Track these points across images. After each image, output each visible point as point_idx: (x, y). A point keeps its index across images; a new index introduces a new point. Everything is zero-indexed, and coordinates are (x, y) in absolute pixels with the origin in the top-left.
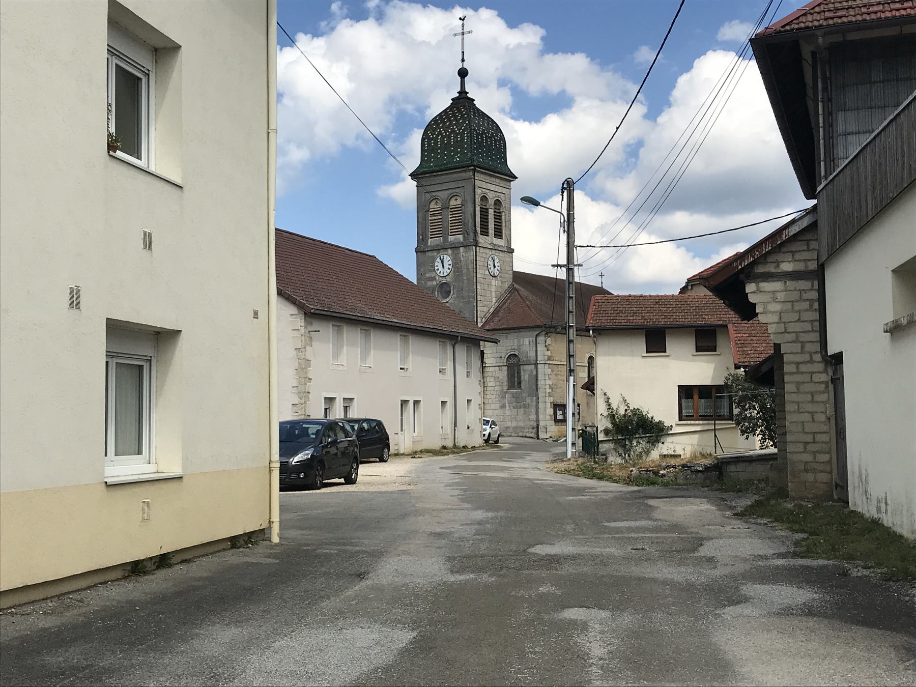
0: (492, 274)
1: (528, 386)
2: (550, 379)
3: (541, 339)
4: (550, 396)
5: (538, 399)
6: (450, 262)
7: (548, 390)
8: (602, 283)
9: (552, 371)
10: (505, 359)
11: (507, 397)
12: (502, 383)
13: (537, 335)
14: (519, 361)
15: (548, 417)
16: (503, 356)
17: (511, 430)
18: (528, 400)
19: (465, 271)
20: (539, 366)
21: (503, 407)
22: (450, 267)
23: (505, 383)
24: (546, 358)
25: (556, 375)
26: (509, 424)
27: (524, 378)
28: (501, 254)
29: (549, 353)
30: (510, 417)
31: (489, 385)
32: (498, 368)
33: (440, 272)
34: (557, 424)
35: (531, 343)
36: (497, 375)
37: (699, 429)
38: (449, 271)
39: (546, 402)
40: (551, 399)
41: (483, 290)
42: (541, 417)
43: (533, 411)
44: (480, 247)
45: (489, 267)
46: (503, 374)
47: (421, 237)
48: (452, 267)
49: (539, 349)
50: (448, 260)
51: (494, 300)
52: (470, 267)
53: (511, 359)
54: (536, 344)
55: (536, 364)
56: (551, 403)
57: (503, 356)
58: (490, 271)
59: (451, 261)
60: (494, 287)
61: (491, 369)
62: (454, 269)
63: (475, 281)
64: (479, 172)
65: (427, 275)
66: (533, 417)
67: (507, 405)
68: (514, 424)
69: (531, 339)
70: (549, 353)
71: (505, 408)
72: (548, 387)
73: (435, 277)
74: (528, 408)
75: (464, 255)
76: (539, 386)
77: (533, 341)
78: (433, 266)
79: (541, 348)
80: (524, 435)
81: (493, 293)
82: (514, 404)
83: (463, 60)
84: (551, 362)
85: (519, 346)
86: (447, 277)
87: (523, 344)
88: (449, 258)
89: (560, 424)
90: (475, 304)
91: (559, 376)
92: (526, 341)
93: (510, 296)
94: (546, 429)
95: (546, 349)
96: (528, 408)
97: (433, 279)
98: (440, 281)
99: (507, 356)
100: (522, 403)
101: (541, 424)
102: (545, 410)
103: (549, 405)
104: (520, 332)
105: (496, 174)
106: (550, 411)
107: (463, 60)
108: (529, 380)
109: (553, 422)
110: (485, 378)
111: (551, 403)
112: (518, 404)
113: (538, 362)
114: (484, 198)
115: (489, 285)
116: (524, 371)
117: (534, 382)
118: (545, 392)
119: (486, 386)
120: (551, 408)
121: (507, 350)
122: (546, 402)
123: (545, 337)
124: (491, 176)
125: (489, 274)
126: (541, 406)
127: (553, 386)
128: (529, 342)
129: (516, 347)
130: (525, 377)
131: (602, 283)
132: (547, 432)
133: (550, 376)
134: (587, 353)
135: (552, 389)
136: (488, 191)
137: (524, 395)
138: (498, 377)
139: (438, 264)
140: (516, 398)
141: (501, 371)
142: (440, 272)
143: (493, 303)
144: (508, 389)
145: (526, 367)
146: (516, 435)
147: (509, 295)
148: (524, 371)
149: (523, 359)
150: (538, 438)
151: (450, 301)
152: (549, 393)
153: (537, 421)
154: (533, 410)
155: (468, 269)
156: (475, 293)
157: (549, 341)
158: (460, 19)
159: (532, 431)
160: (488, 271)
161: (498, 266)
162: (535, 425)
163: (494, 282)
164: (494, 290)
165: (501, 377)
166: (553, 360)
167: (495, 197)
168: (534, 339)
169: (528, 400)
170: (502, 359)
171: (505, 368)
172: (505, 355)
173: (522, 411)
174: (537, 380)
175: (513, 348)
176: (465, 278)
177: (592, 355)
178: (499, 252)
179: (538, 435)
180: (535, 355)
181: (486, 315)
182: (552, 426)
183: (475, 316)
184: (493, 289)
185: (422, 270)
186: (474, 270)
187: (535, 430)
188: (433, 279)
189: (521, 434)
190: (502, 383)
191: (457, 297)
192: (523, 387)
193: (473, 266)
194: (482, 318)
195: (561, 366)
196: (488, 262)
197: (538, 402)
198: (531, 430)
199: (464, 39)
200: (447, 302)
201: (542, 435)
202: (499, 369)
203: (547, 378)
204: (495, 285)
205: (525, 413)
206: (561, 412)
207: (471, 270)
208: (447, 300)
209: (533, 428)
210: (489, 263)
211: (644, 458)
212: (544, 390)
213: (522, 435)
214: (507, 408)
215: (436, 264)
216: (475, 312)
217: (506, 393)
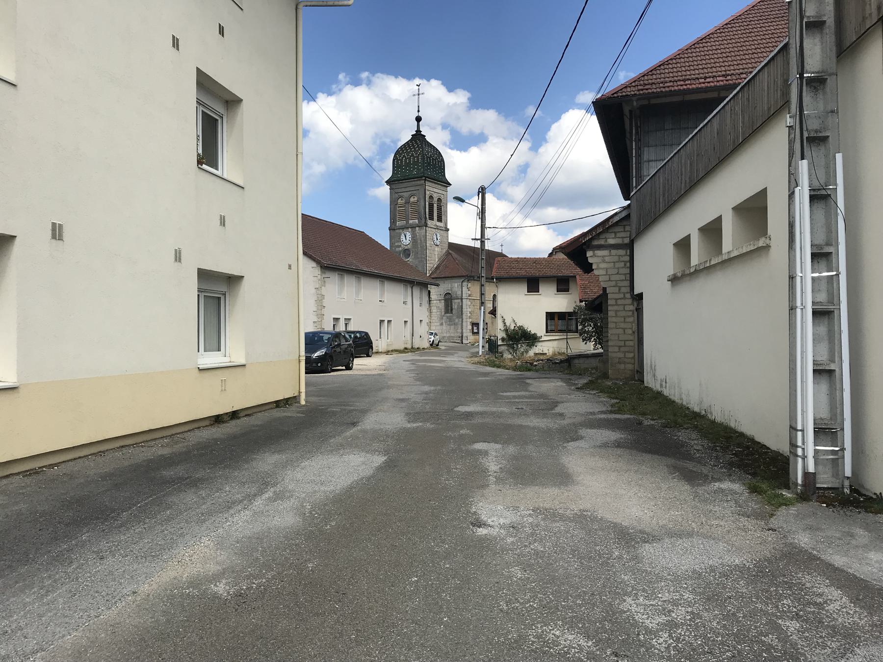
2: (469, 308)
6: (410, 236)
9: (472, 303)
15: (468, 331)
17: (446, 338)
18: (457, 321)
19: (419, 242)
21: (442, 324)
23: (443, 310)
25: (474, 306)
26: (445, 335)
28: (441, 232)
29: (469, 292)
40: (471, 320)
46: (442, 305)
50: (409, 235)
52: (423, 239)
61: (435, 302)
65: (396, 244)
66: (460, 331)
67: (444, 323)
70: (469, 292)
76: (463, 312)
78: (400, 238)
79: (465, 289)
81: (436, 256)
82: (448, 323)
84: (470, 298)
85: (452, 288)
94: (467, 337)
97: (400, 246)
101: (464, 335)
102: (467, 327)
103: (469, 323)
106: (470, 327)
107: (419, 111)
114: (431, 197)
115: (434, 250)
117: (460, 309)
126: (464, 324)
130: (455, 306)
139: (403, 237)
150: (462, 343)
153: (462, 333)
157: (470, 285)
162: (461, 335)
163: (437, 249)
168: (461, 284)
169: (457, 321)
173: (452, 327)
174: (462, 308)
184: (436, 253)
188: (400, 246)
189: (452, 341)
201: (464, 341)
203: (468, 307)
206: (476, 328)
209: (459, 337)
211: (525, 355)
215: (402, 237)
217: (444, 316)
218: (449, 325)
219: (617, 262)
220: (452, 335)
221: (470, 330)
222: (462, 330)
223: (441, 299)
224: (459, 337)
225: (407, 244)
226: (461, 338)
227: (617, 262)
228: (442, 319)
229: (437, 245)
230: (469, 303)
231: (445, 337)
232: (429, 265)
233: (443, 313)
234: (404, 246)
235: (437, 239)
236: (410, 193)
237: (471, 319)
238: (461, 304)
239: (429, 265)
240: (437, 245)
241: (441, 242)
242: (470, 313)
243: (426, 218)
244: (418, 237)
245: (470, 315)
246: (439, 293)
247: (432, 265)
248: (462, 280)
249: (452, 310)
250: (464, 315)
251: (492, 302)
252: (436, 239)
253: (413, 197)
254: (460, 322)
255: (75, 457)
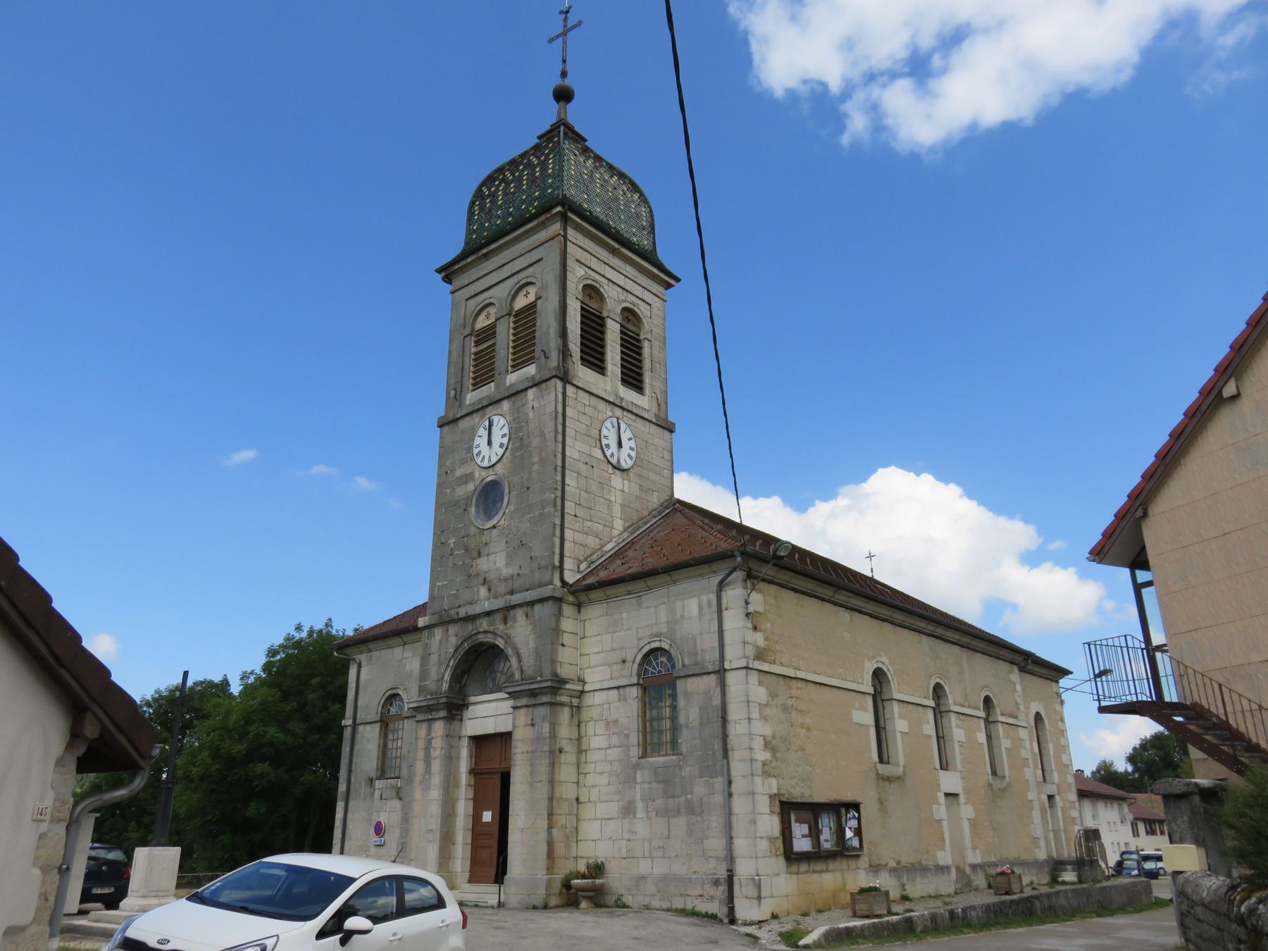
0: (614, 461)
1: (698, 741)
2: (764, 718)
3: (734, 594)
4: (767, 774)
5: (730, 782)
6: (506, 430)
7: (762, 755)
8: (872, 569)
9: (773, 695)
10: (636, 666)
11: (639, 778)
12: (627, 735)
13: (721, 585)
14: (673, 666)
15: (763, 845)
16: (629, 657)
17: (650, 888)
18: (699, 789)
19: (535, 441)
20: (731, 678)
21: (628, 810)
22: (505, 441)
23: (634, 739)
24: (750, 651)
25: (785, 709)
26: (644, 867)
27: (688, 717)
28: (640, 424)
29: (759, 639)
30: (646, 844)
31: (592, 746)
32: (615, 692)
33: (484, 457)
34: (794, 868)
35: (706, 610)
36: (614, 716)
37: (435, 794)
38: (500, 452)
39: (753, 794)
40: (773, 785)
41: (586, 491)
42: (740, 844)
43: (714, 825)
44: (578, 387)
45: (604, 442)
46: (627, 710)
47: (453, 393)
48: (510, 439)
49: (728, 625)
50: (501, 427)
51: (619, 525)
52: (549, 428)
53: (649, 663)
54: (720, 611)
55: (721, 672)
56: (772, 797)
57: (629, 657)
58: (608, 453)
59: (507, 426)
60: (618, 493)
61: (599, 698)
62: (513, 444)
63: (559, 463)
64: (578, 228)
65: (458, 473)
66: (716, 844)
67: (640, 804)
68: (659, 868)
69: (704, 599)
70: (759, 639)
71: (635, 814)
72: (758, 743)
73: (472, 474)
74: (700, 814)
75: (536, 405)
76: (733, 741)
77: (709, 606)
78: (470, 449)
79: (734, 621)
80: (689, 906)
81: (617, 510)
82: (660, 801)
83: (564, 74)
84: (765, 667)
85: (672, 623)
86: (499, 468)
87: (683, 617)
88: (503, 421)
89: (804, 867)
90: (558, 521)
91: (794, 714)
92: (692, 606)
93: (661, 523)
94: (758, 886)
95: (750, 625)
96: (700, 814)
97: (468, 478)
98: (483, 479)
99: (640, 656)
100: (683, 799)
101: (744, 869)
102: (754, 822)
103: (764, 804)
104: (674, 582)
105: (624, 250)
106: (770, 824)
107: (564, 74)
108: (701, 724)
109: (782, 860)
110: (583, 725)
111: (772, 797)
112: (671, 801)
113: (727, 666)
114: (591, 291)
115: (604, 484)
116: (688, 695)
117: (717, 727)
118: (752, 760)
119: (584, 748)
120: (772, 812)
121: (639, 639)
122: (753, 794)
123: (746, 588)
124: (613, 251)
125: (602, 457)
126: (739, 805)
127: (774, 742)
128: (701, 608)
129: (664, 629)
130: (690, 713)
131: (872, 569)
132: (759, 898)
133: (768, 711)
134: (870, 659)
135: (774, 751)
136: (606, 281)
137: (687, 771)
138: (616, 721)
139: (481, 441)
140: (667, 782)
141: (625, 700)
142: (484, 457)
143: (615, 533)
144: (644, 756)
145: (694, 685)
146: (665, 905)
147: (662, 520)
148: (688, 695)
149: (683, 660)
150: (733, 921)
151: (502, 522)
152: (764, 764)
153: (730, 858)
154: (716, 821)
155: (542, 434)
156: (559, 493)
157: (758, 601)
158: (561, 12)
159: (712, 893)
160: (600, 451)
161: (631, 449)
162: (722, 873)
163: (617, 481)
164: (619, 501)
165: (624, 721)
166: (774, 663)
167: (625, 301)
168: (713, 597)
169: (699, 789)
170: (627, 665)
171: (634, 692)
172: (634, 654)
173: (680, 823)
174: (724, 720)
175: (655, 630)
176: (536, 459)
177: (880, 665)
178: (634, 418)
179: (731, 910)
180: (717, 644)
181: (591, 555)
182: (777, 875)
183: (557, 550)
184: (617, 498)
185: (448, 464)
186: (556, 438)
187: (722, 890)
188: (468, 478)
189: (678, 903)
190: (627, 735)
191: (517, 510)
192: (684, 749)
193: (556, 425)
194: (580, 562)
195: (800, 684)
196: (600, 431)
197: (730, 795)
198: (710, 890)
199: (566, 42)
200: (494, 527)
201: (745, 910)
202: (619, 694)
203: (755, 714)
204: (623, 491)
205: (690, 832)
206: (804, 828)
207: (550, 436)
208: (494, 521)
209: (716, 883)
210: (604, 432)
211: (466, 668)
212: (746, 754)
213: (680, 906)
214: (638, 816)
215: (477, 441)
216: (557, 541)
217: (636, 767)
218: (666, 813)
219: (599, 840)
220: (679, 869)
221: (771, 840)
222: (730, 839)
223: (624, 682)
224: (716, 883)
225: (494, 460)
226: (723, 888)
227: (599, 840)
228: (629, 781)
229: (617, 468)
230: (759, 693)
231: (642, 878)
232: (580, 538)
233: (635, 752)
234: (484, 473)
235: (620, 445)
236: (514, 279)
237: (773, 781)
238: (717, 701)
239: (580, 538)
240: (617, 468)
241: (638, 462)
242: (767, 745)
243: (565, 352)
244: (532, 426)
245: (766, 756)
246: (617, 656)
247: (592, 542)
248: (719, 578)
249: (675, 729)
250: (736, 756)
251: (870, 701)
252: (613, 442)
253: (524, 292)
254: (719, 799)
255: (545, 855)
